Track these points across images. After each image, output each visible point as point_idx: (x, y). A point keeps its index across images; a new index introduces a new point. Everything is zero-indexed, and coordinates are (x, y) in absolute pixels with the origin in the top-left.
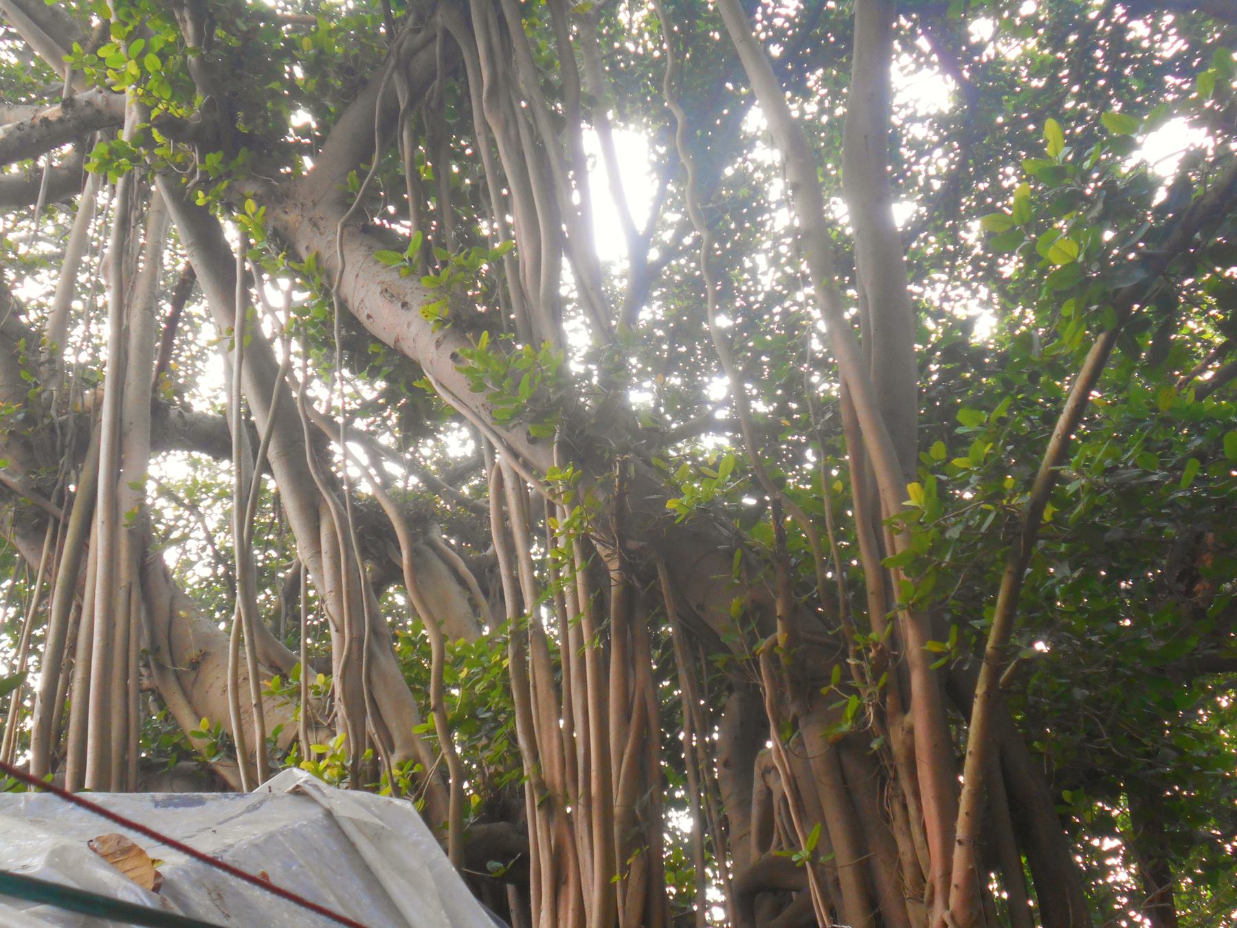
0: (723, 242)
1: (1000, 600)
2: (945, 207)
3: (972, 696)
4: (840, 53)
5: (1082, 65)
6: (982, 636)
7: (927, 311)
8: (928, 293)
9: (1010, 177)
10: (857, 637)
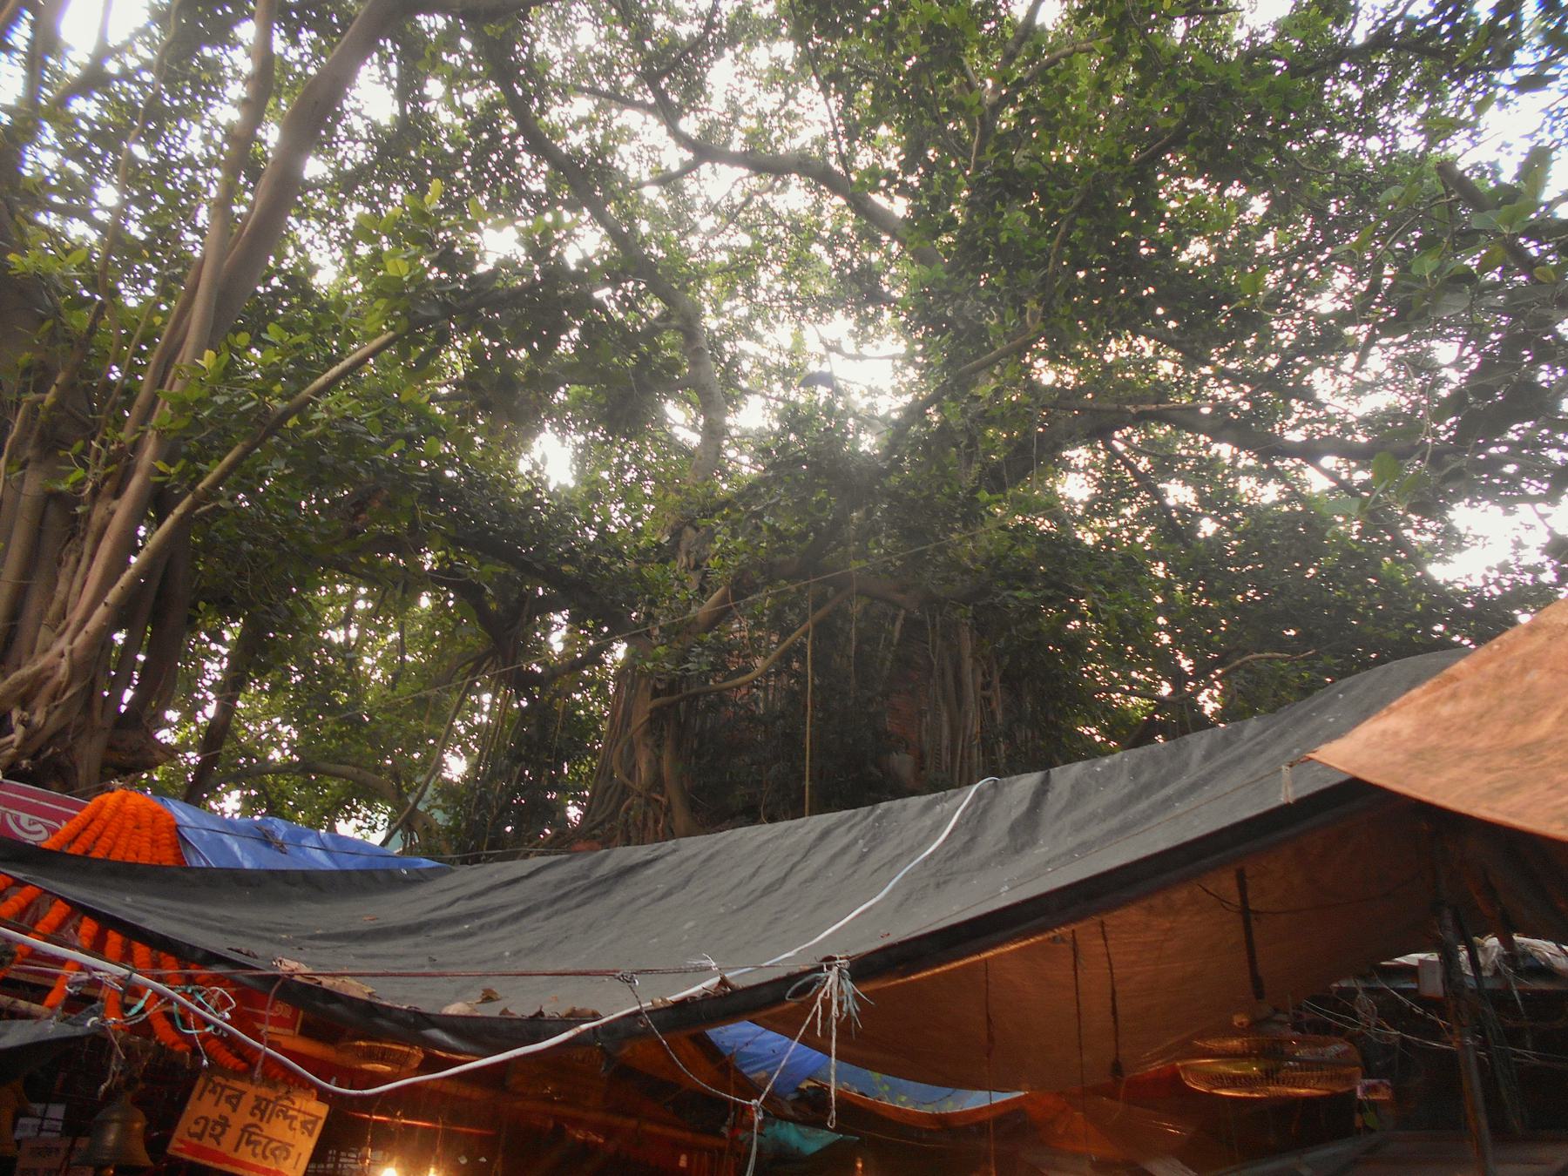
0: (173, 97)
1: (227, 459)
2: (346, 183)
3: (171, 512)
4: (335, 34)
5: (479, 159)
6: (201, 475)
7: (293, 242)
8: (301, 231)
9: (398, 193)
10: (109, 430)
